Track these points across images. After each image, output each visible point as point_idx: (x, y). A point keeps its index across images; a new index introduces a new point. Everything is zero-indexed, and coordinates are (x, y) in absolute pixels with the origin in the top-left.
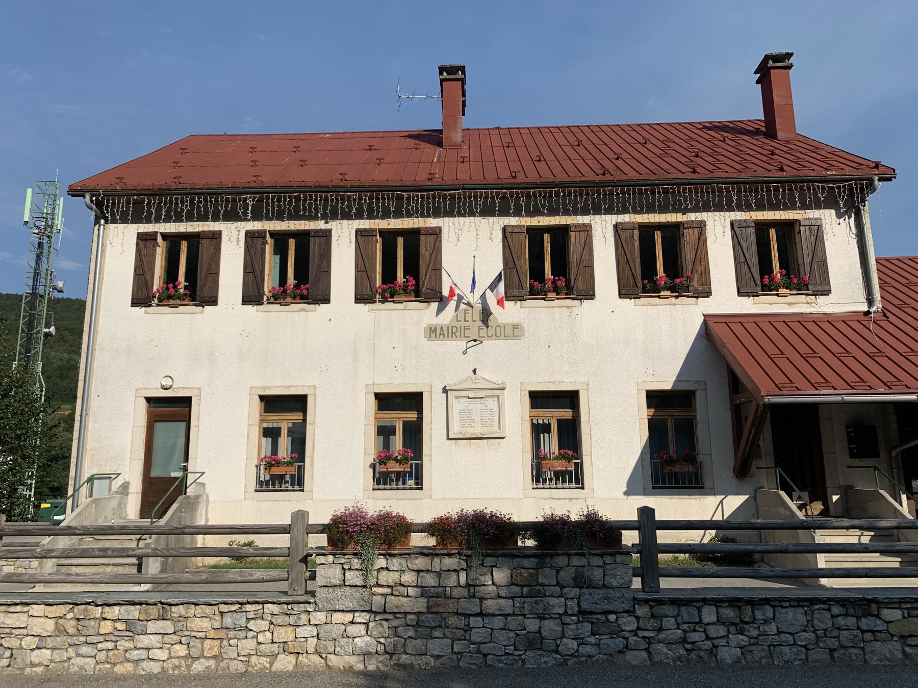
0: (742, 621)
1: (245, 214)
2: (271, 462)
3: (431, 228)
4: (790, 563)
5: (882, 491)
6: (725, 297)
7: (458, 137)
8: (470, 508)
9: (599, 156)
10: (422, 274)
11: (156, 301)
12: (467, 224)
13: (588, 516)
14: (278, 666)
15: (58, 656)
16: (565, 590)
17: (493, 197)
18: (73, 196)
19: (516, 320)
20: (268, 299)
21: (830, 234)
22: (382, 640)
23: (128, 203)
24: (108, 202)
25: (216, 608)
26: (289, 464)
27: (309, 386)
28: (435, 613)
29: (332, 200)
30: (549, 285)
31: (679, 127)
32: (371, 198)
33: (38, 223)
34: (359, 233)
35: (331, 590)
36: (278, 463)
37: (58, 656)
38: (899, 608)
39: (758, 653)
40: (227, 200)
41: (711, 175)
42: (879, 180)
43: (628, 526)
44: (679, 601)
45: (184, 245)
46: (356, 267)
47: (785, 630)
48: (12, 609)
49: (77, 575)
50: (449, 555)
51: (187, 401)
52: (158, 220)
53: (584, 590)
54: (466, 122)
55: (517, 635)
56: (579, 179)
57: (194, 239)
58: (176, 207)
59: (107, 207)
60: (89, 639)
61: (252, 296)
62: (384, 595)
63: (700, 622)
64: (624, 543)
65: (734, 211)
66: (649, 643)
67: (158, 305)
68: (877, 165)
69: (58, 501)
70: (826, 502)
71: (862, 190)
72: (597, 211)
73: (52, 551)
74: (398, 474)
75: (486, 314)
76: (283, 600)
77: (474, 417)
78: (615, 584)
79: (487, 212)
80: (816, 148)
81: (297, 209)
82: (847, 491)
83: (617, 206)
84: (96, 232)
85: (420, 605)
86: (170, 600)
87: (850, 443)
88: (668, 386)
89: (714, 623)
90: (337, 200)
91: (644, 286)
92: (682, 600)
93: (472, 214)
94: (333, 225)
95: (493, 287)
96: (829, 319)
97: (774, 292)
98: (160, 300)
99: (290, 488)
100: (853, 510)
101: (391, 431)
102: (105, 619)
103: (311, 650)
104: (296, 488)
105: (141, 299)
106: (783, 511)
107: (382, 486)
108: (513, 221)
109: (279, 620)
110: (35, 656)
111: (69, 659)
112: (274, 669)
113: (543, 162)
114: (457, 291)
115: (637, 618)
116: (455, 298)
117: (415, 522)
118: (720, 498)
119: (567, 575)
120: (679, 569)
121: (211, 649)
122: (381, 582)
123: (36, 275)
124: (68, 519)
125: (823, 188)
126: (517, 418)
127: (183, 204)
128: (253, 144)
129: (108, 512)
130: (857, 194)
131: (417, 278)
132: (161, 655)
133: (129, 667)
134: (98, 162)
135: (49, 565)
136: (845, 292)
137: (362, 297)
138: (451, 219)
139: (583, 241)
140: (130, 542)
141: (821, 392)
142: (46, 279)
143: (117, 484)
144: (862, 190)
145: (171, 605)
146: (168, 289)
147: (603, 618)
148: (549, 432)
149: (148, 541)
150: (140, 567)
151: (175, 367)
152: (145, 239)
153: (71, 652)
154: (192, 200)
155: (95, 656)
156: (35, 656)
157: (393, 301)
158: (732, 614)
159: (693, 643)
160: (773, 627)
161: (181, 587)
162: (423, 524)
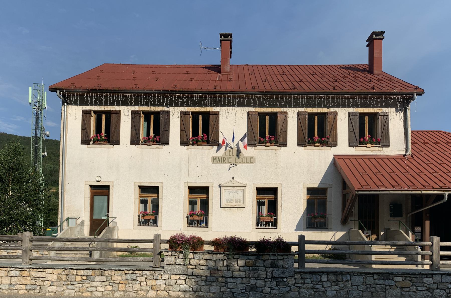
0: (337, 281)
1: (131, 103)
2: (144, 214)
3: (215, 112)
4: (360, 258)
5: (401, 231)
6: (343, 148)
7: (228, 69)
8: (229, 235)
9: (293, 80)
10: (210, 133)
11: (92, 142)
12: (231, 111)
13: (278, 240)
14: (149, 295)
15: (59, 289)
16: (267, 269)
17: (243, 98)
18: (51, 91)
19: (252, 155)
20: (142, 142)
21: (392, 120)
22: (192, 286)
23: (77, 95)
24: (68, 95)
25: (123, 272)
26: (152, 215)
28: (213, 276)
29: (170, 97)
30: (267, 139)
31: (329, 67)
32: (188, 97)
33: (35, 104)
34: (182, 113)
35: (170, 266)
36: (147, 215)
37: (59, 289)
39: (343, 293)
40: (123, 96)
41: (341, 91)
42: (416, 95)
43: (294, 244)
44: (312, 273)
45: (104, 116)
46: (181, 129)
47: (354, 284)
48: (39, 270)
49: (65, 257)
50: (220, 254)
51: (107, 187)
52: (91, 104)
53: (274, 269)
54: (232, 61)
56: (283, 90)
57: (108, 114)
58: (100, 98)
59: (68, 97)
60: (72, 283)
61: (135, 141)
62: (193, 269)
63: (320, 281)
64: (292, 251)
65: (350, 107)
66: (299, 289)
67: (93, 144)
68: (417, 88)
69: (54, 228)
70: (378, 235)
71: (408, 99)
72: (290, 106)
73: (54, 247)
74: (198, 221)
75: (239, 152)
76: (151, 269)
77: (232, 198)
78: (287, 267)
79: (241, 105)
80: (390, 78)
81: (154, 101)
82: (387, 231)
83: (299, 104)
84: (63, 109)
85: (208, 273)
86: (104, 269)
88: (316, 186)
89: (326, 281)
90: (172, 97)
91: (309, 141)
92: (314, 272)
93: (233, 106)
94: (170, 109)
95: (242, 140)
96: (388, 158)
97: (365, 145)
98: (94, 142)
99: (152, 225)
100: (389, 238)
101: (195, 203)
102: (78, 275)
103: (163, 289)
104: (155, 225)
105: (85, 141)
106: (359, 238)
107: (191, 226)
108: (252, 109)
109: (150, 277)
110: (50, 289)
111: (64, 290)
112: (147, 296)
113: (267, 82)
114: (226, 142)
115: (295, 279)
116: (225, 144)
117: (206, 240)
118: (334, 232)
119: (268, 263)
120: (313, 260)
121: (122, 288)
123: (36, 128)
124: (59, 235)
125: (391, 98)
126: (251, 199)
127: (102, 97)
128: (134, 69)
129: (76, 233)
130: (406, 101)
131: (208, 135)
132: (102, 289)
133: (89, 294)
134: (63, 75)
135: (53, 253)
136: (396, 146)
137: (184, 143)
138: (224, 108)
139: (283, 119)
140: (86, 245)
141: (381, 189)
142: (41, 130)
143: (79, 221)
144: (408, 99)
145: (105, 270)
146: (97, 136)
147: (282, 280)
148: (264, 205)
149: (94, 245)
150: (91, 255)
151: (102, 172)
152: (85, 113)
153: (65, 288)
154: (107, 95)
155: (74, 289)
156: (50, 289)
157: (197, 145)
158: (334, 278)
159: (317, 289)
160: (350, 283)
161: (108, 263)
162: (209, 241)
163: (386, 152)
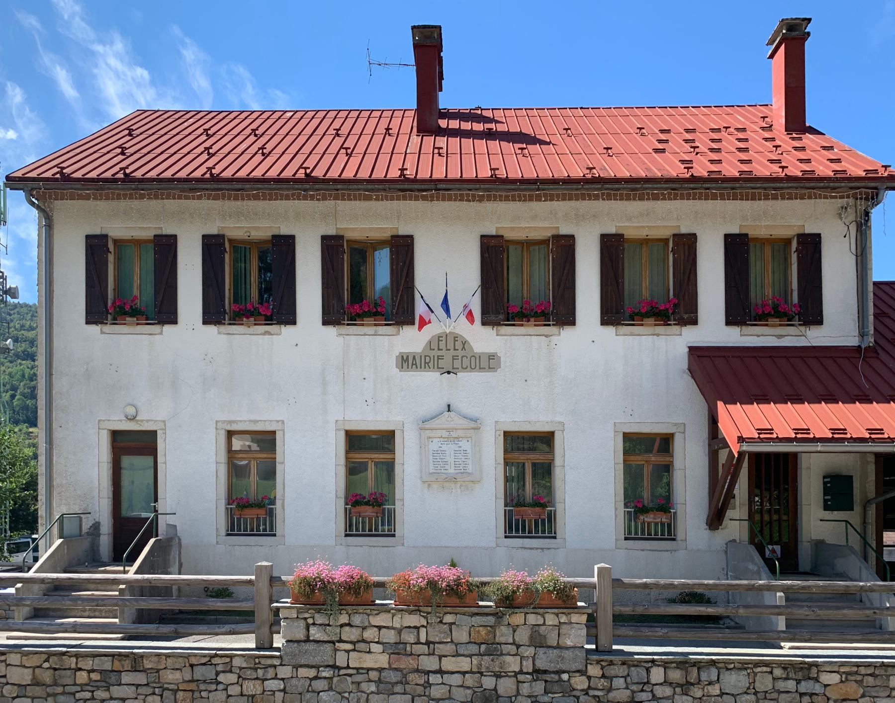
0: (687, 682)
6: (713, 328)
16: (521, 649)
27: (278, 421)
38: (838, 672)
55: (475, 692)
60: (68, 689)
61: (213, 314)
63: (648, 682)
77: (447, 459)
87: (825, 494)
89: (661, 684)
102: (80, 669)
115: (589, 678)
119: (523, 636)
122: (343, 638)
147: (556, 677)
163: (816, 337)
